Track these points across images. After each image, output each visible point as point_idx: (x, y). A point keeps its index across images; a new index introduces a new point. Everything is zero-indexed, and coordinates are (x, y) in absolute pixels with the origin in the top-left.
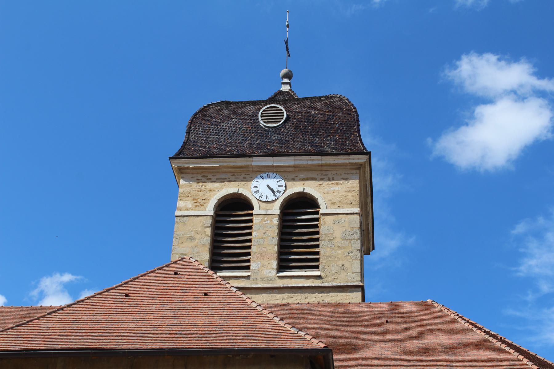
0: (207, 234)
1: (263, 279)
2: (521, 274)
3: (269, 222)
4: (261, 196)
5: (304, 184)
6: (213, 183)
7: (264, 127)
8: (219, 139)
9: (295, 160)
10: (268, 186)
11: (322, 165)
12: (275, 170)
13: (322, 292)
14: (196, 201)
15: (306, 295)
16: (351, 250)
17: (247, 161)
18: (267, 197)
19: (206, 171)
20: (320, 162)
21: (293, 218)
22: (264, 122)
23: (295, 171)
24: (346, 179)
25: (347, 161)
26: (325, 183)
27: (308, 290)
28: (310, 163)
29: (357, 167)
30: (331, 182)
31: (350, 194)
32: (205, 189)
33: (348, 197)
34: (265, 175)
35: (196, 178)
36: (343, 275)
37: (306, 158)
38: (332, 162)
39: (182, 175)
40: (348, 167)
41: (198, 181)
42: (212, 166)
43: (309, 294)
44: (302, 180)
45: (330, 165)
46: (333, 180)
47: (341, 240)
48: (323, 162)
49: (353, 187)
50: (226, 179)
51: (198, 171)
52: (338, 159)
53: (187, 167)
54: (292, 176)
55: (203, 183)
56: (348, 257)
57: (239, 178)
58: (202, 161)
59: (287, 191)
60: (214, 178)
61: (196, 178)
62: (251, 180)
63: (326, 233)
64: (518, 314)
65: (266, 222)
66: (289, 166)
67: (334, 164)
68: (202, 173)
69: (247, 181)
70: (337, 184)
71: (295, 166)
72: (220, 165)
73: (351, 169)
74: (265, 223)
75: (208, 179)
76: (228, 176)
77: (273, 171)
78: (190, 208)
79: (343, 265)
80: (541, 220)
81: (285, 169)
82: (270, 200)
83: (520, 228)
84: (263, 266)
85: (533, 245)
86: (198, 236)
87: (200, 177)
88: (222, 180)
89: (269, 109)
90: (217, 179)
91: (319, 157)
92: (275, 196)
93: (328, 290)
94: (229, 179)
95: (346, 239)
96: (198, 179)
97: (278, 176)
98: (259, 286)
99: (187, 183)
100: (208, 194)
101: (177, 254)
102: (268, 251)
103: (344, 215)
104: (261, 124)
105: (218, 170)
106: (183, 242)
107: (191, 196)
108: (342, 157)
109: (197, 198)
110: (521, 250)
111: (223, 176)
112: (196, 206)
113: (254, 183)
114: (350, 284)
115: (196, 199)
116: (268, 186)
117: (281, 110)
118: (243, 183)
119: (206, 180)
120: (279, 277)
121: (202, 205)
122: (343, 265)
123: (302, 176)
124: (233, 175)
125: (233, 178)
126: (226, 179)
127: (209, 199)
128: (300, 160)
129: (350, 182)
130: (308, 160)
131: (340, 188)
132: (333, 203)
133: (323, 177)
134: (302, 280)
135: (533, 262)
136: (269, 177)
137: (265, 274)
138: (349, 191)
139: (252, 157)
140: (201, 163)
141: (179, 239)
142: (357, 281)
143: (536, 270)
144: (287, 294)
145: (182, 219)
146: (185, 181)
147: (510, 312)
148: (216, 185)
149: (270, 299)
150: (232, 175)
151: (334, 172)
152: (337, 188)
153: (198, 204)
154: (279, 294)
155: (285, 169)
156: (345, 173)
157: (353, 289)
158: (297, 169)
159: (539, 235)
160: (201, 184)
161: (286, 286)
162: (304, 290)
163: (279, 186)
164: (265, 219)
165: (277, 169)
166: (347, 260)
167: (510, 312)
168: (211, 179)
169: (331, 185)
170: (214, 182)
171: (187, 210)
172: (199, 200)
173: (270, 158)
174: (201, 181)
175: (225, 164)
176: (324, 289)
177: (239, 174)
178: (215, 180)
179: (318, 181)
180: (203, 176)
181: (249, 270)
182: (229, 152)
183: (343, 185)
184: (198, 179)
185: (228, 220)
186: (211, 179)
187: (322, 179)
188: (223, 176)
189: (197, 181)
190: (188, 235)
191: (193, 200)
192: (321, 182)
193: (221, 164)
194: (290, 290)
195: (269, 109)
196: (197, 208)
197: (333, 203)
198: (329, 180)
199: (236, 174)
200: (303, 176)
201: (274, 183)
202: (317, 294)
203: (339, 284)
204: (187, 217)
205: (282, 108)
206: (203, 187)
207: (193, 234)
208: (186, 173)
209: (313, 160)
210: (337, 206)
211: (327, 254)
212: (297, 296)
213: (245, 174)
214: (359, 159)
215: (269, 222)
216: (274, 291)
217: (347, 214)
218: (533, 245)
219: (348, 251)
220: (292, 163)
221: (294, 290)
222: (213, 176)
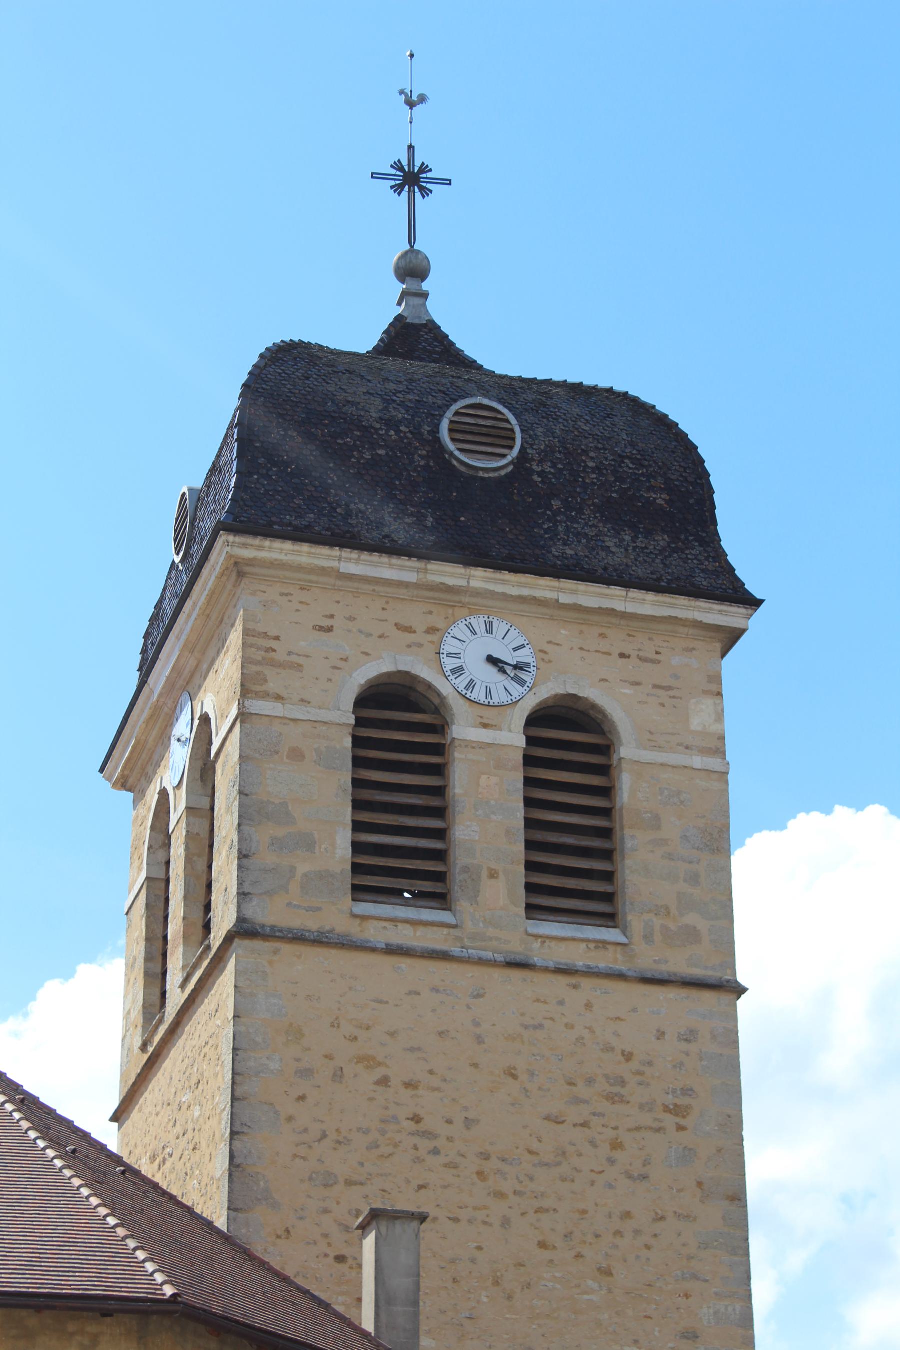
4: (471, 685)
18: (489, 692)
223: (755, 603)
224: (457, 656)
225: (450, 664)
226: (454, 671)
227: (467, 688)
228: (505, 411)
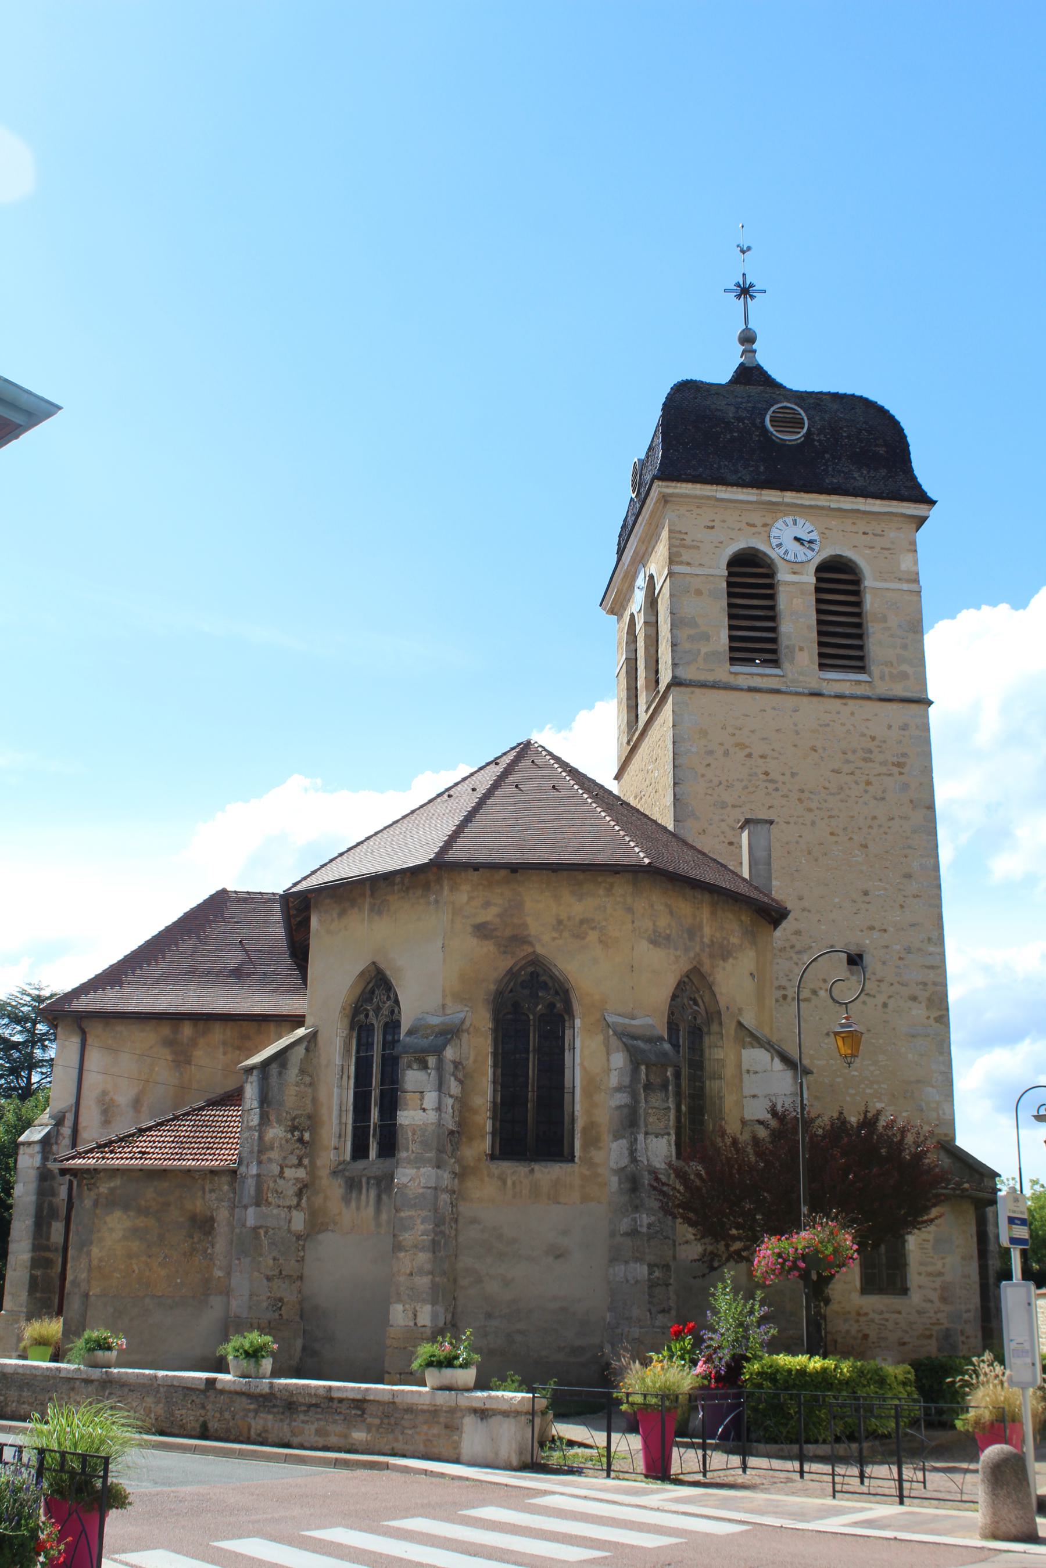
4: (786, 552)
18: (796, 556)
82: (799, 560)
223: (932, 503)
224: (778, 537)
225: (775, 542)
226: (777, 546)
227: (784, 554)
228: (799, 409)
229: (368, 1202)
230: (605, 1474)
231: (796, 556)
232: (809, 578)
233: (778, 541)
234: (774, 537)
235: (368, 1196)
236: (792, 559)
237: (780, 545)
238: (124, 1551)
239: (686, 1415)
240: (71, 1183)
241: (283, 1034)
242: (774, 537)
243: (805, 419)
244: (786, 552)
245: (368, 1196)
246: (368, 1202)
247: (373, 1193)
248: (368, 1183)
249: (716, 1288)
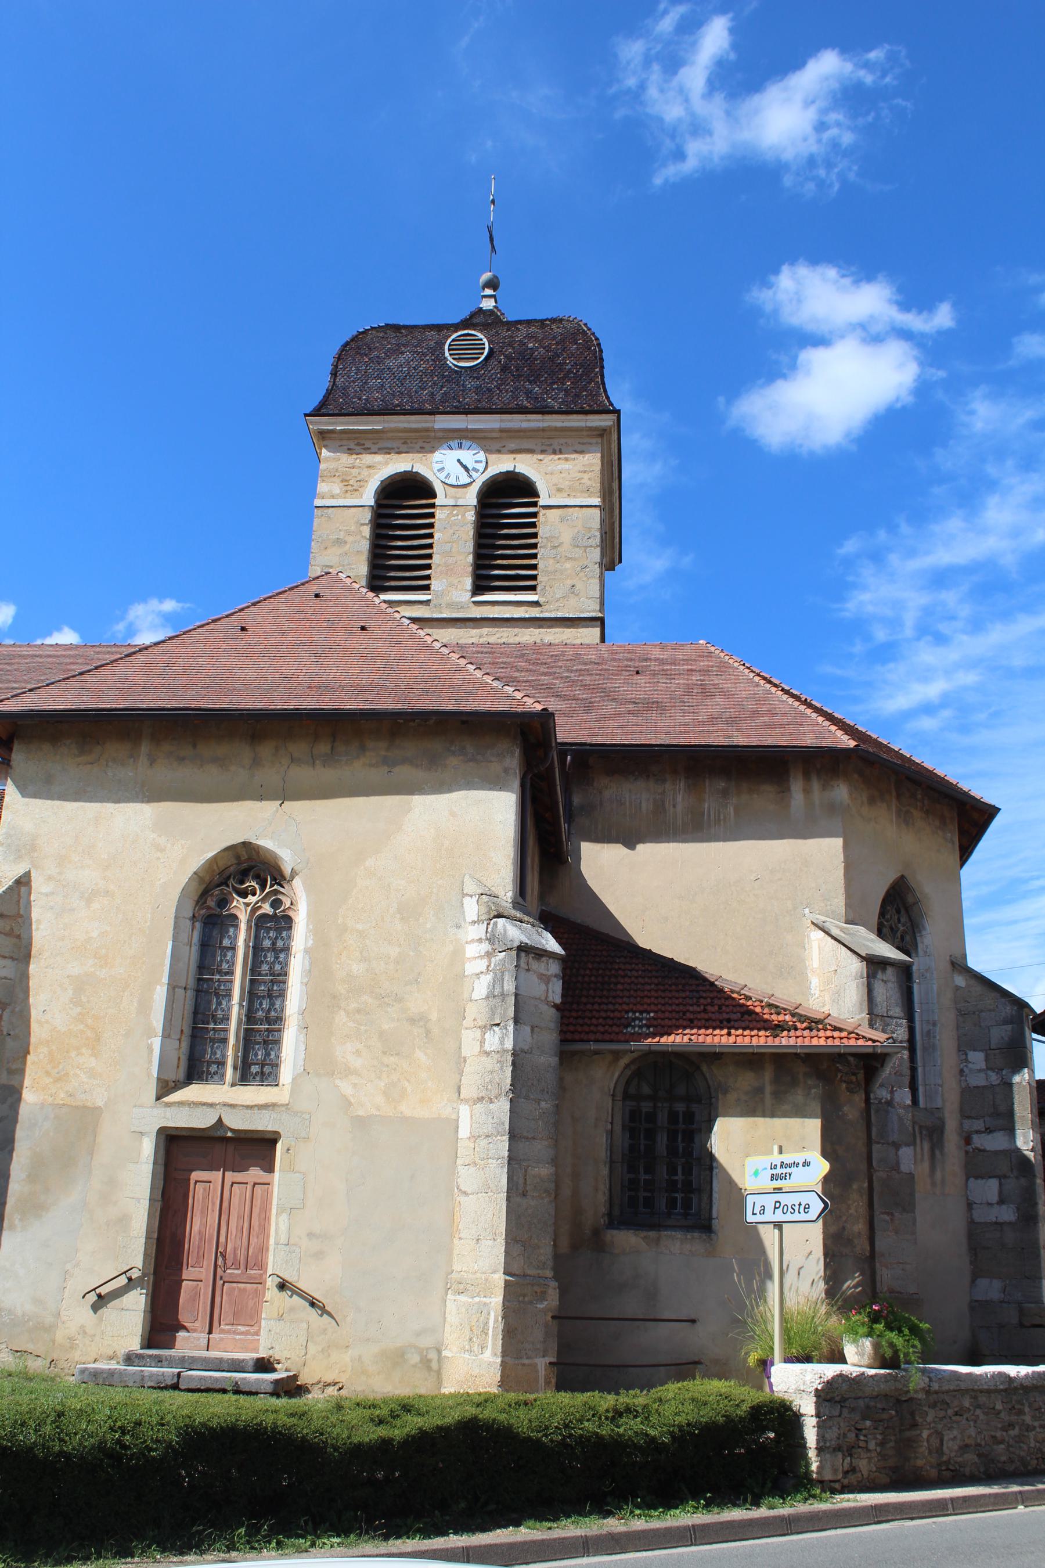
0: (363, 535)
1: (450, 606)
2: (847, 614)
3: (460, 517)
4: (448, 476)
5: (514, 459)
6: (373, 455)
7: (453, 367)
8: (382, 385)
9: (501, 421)
10: (459, 461)
11: (543, 430)
12: (470, 435)
13: (540, 627)
14: (346, 484)
15: (516, 630)
16: (586, 562)
17: (426, 422)
18: (458, 478)
19: (363, 435)
20: (541, 425)
21: (498, 512)
22: (454, 359)
23: (501, 438)
24: (581, 452)
25: (583, 424)
26: (548, 458)
27: (519, 623)
28: (525, 425)
29: (598, 433)
30: (557, 457)
31: (586, 476)
32: (360, 465)
33: (583, 481)
34: (454, 443)
35: (346, 447)
36: (573, 601)
37: (517, 418)
38: (559, 424)
39: (325, 443)
40: (585, 433)
41: (350, 451)
42: (371, 428)
43: (520, 630)
44: (512, 452)
45: (556, 429)
46: (561, 453)
47: (571, 547)
48: (546, 425)
49: (591, 465)
50: (393, 449)
51: (350, 435)
52: (569, 421)
53: (332, 430)
54: (497, 445)
55: (357, 454)
56: (582, 574)
57: (413, 448)
58: (356, 420)
59: (489, 469)
60: (374, 448)
61: (346, 447)
62: (432, 451)
63: (547, 535)
64: (839, 672)
65: (456, 518)
66: (492, 430)
67: (562, 427)
68: (356, 438)
69: (427, 452)
70: (566, 459)
71: (502, 431)
72: (384, 428)
73: (588, 436)
74: (453, 518)
75: (364, 449)
76: (394, 444)
77: (467, 438)
78: (338, 495)
79: (573, 586)
80: (882, 535)
81: (486, 434)
82: (461, 483)
83: (850, 546)
84: (451, 585)
85: (867, 572)
86: (350, 539)
87: (352, 446)
88: (388, 451)
89: (462, 338)
90: (379, 449)
91: (539, 417)
92: (471, 476)
93: (548, 623)
94: (398, 448)
95: (578, 546)
96: (349, 449)
97: (474, 445)
98: (444, 616)
99: (332, 454)
100: (365, 472)
101: (318, 566)
102: (459, 562)
103: (577, 508)
104: (448, 362)
105: (381, 435)
106: (326, 548)
107: (339, 476)
108: (574, 417)
109: (348, 479)
110: (850, 578)
111: (389, 444)
112: (347, 491)
113: (437, 456)
114: (582, 615)
115: (346, 481)
116: (459, 461)
117: (481, 340)
118: (421, 455)
119: (362, 451)
120: (474, 603)
121: (356, 490)
122: (573, 586)
123: (513, 446)
124: (405, 443)
125: (404, 448)
126: (393, 449)
127: (367, 481)
128: (510, 421)
129: (587, 456)
130: (521, 421)
131: (571, 467)
132: (559, 490)
133: (544, 448)
134: (523, 608)
135: (865, 597)
136: (460, 447)
137: (454, 597)
138: (585, 472)
139: (435, 415)
140: (354, 424)
141: (321, 543)
142: (594, 611)
143: (870, 609)
144: (487, 629)
145: (326, 511)
146: (329, 452)
147: (828, 669)
148: (378, 458)
149: (461, 636)
150: (403, 443)
151: (562, 441)
152: (567, 466)
153: (349, 488)
154: (474, 628)
155: (486, 434)
156: (579, 443)
157: (588, 623)
158: (505, 435)
159: (877, 557)
160: (355, 456)
161: (486, 616)
162: (513, 623)
163: (476, 462)
164: (454, 512)
165: (473, 434)
166: (580, 579)
167: (828, 669)
168: (369, 449)
169: (557, 461)
170: (375, 453)
171: (333, 497)
172: (351, 482)
173: (463, 417)
174: (355, 451)
175: (393, 425)
176: (543, 622)
177: (415, 441)
178: (376, 450)
179: (537, 454)
180: (358, 444)
181: (428, 592)
182: (398, 405)
183: (576, 462)
184: (349, 449)
185: (398, 514)
186: (369, 449)
187: (543, 452)
188: (389, 444)
189: (349, 452)
190: (334, 537)
191: (342, 481)
192: (541, 457)
193: (386, 425)
194: (490, 622)
195: (462, 338)
196: (348, 495)
197: (559, 490)
198: (554, 453)
199: (408, 441)
200: (513, 445)
201: (471, 456)
202: (532, 629)
203: (567, 615)
204: (333, 509)
205: (482, 337)
206: (358, 461)
207: (342, 535)
208: (330, 439)
209: (529, 421)
210: (566, 495)
211: (549, 569)
212: (503, 631)
213: (424, 442)
214: (600, 420)
215: (460, 517)
216: (468, 624)
217: (581, 507)
218: (867, 572)
219: (581, 564)
220: (496, 425)
221: (498, 623)
222: (374, 443)
225: (437, 467)
226: (439, 471)
227: (446, 478)
229: (922, 1155)
230: (270, 1186)
231: (458, 478)
232: (471, 497)
233: (440, 466)
234: (437, 462)
235: (922, 1149)
236: (454, 483)
237: (442, 470)
238: (846, 752)
239: (491, 987)
240: (838, 1423)
241: (880, 277)
242: (437, 462)
243: (446, 347)
244: (448, 476)
245: (922, 1149)
246: (922, 1155)
247: (926, 1146)
248: (921, 1133)
249: (787, 1497)
